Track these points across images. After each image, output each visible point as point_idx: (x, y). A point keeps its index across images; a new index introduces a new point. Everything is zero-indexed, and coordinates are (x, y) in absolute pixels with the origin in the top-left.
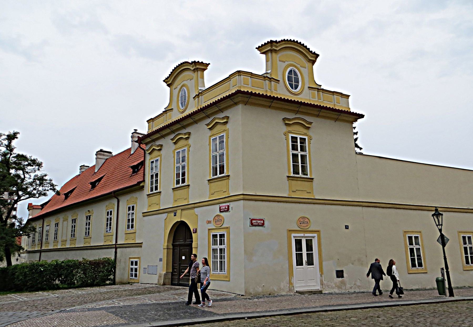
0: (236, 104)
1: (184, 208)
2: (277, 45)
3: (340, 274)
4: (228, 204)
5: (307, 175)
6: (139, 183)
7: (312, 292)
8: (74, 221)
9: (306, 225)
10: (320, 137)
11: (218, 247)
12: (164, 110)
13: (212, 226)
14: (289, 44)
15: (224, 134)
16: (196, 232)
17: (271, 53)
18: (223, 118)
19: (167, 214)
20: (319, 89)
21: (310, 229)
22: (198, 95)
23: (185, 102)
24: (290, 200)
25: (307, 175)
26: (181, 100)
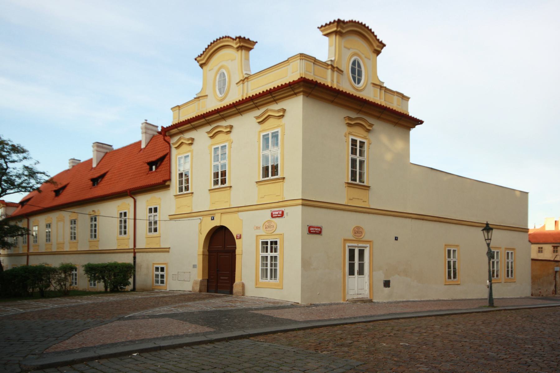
0: (296, 94)
1: (226, 211)
2: (344, 26)
3: (387, 284)
4: (283, 209)
5: (363, 182)
6: (165, 181)
7: (363, 300)
8: (74, 222)
10: (381, 141)
11: (269, 254)
12: (196, 96)
14: (356, 27)
15: (279, 130)
16: (240, 238)
17: (336, 35)
18: (279, 111)
20: (381, 87)
21: (363, 239)
22: (243, 80)
23: (224, 88)
25: (363, 182)
26: (219, 85)
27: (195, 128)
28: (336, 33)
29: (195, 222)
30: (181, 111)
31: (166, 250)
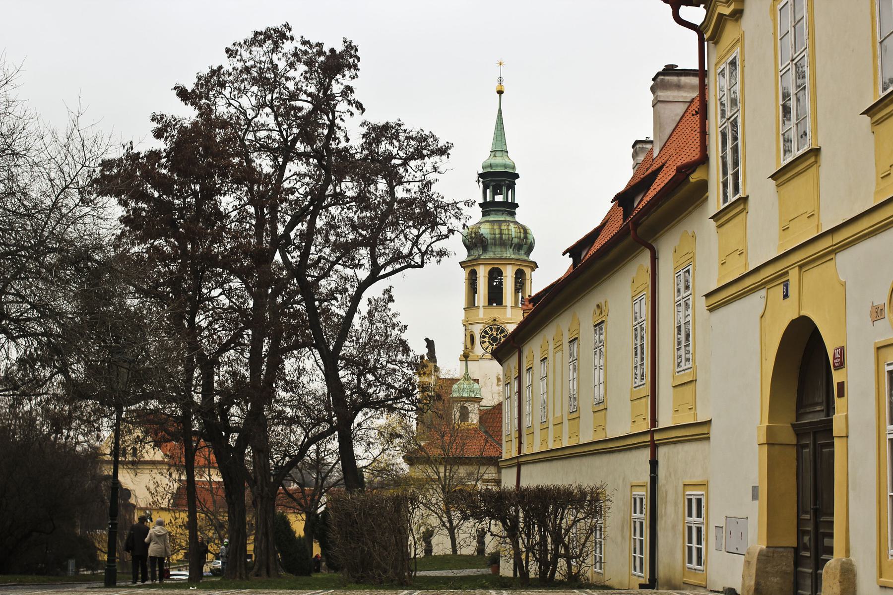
19: (763, 292)
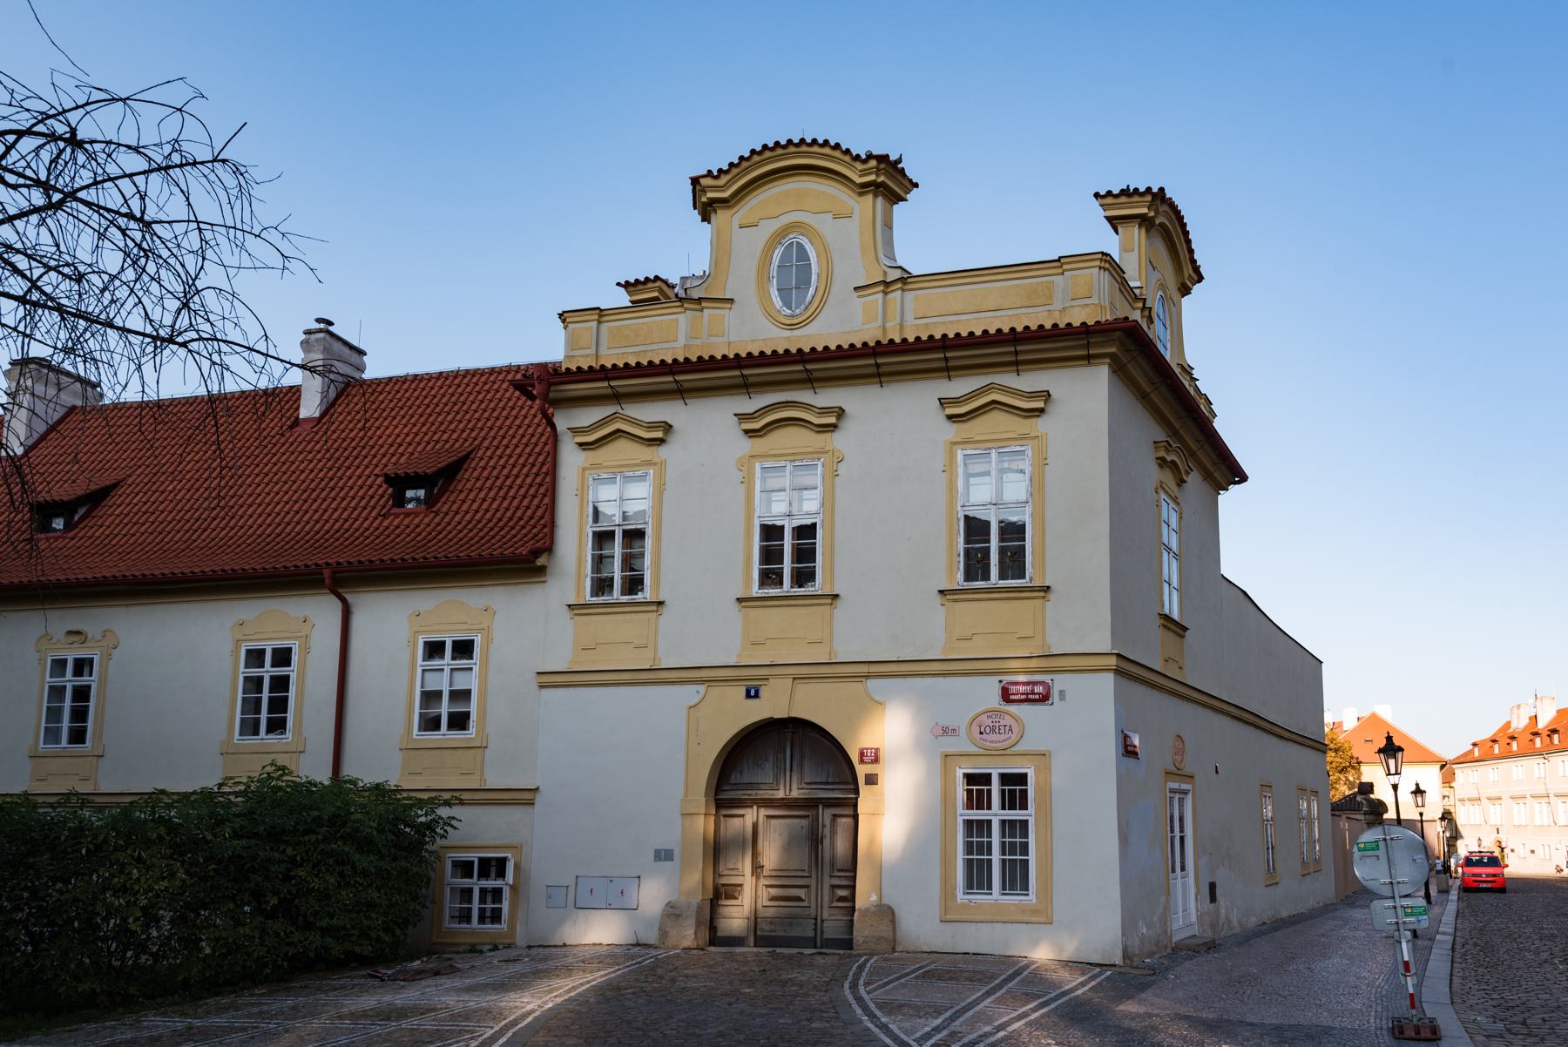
0: (1089, 359)
9: (1003, 737)
13: (962, 744)
17: (875, 196)
19: (702, 688)
24: (1161, 681)
27: (681, 393)
28: (1143, 220)
29: (669, 705)
30: (604, 326)
31: (523, 798)
